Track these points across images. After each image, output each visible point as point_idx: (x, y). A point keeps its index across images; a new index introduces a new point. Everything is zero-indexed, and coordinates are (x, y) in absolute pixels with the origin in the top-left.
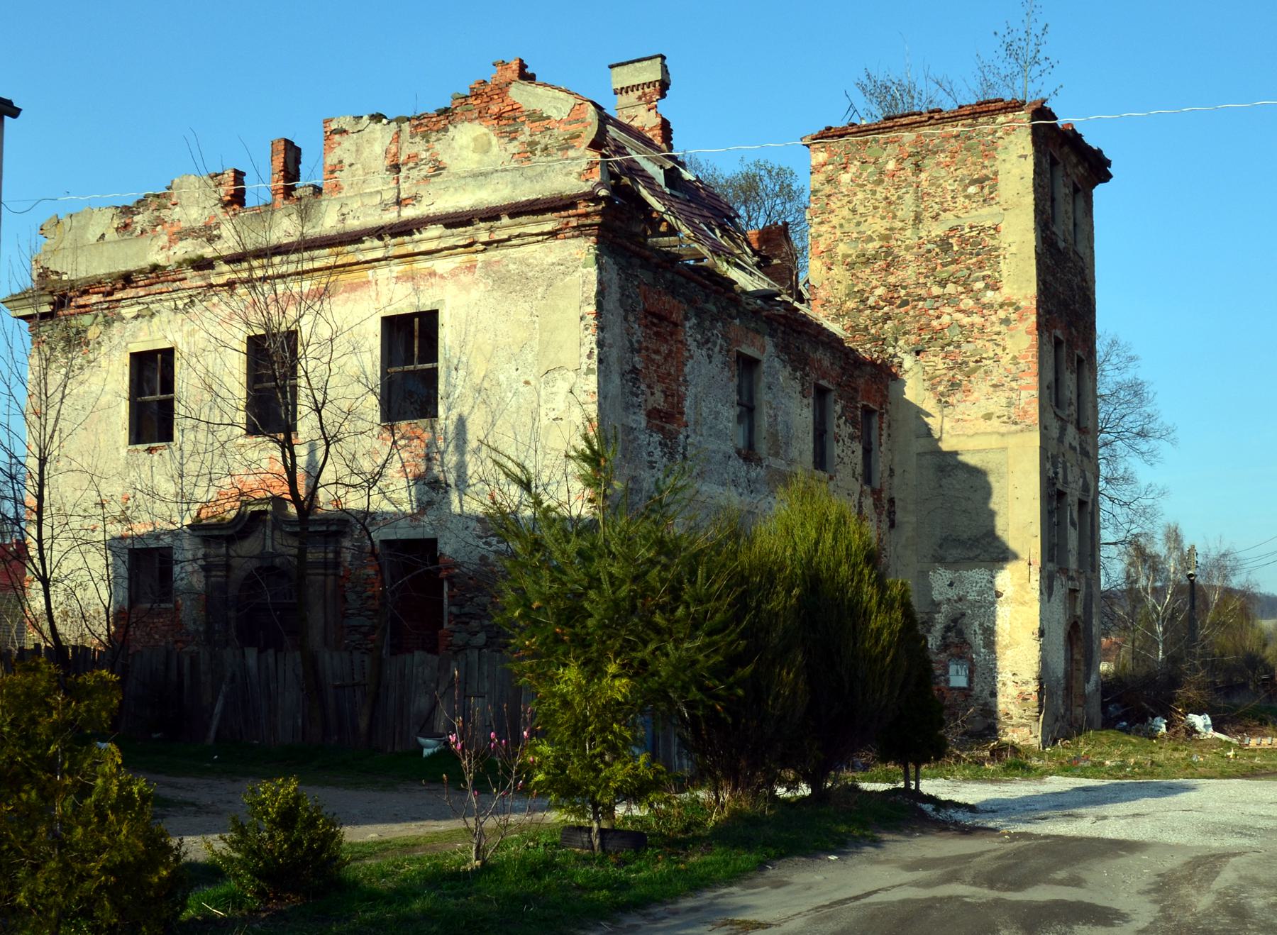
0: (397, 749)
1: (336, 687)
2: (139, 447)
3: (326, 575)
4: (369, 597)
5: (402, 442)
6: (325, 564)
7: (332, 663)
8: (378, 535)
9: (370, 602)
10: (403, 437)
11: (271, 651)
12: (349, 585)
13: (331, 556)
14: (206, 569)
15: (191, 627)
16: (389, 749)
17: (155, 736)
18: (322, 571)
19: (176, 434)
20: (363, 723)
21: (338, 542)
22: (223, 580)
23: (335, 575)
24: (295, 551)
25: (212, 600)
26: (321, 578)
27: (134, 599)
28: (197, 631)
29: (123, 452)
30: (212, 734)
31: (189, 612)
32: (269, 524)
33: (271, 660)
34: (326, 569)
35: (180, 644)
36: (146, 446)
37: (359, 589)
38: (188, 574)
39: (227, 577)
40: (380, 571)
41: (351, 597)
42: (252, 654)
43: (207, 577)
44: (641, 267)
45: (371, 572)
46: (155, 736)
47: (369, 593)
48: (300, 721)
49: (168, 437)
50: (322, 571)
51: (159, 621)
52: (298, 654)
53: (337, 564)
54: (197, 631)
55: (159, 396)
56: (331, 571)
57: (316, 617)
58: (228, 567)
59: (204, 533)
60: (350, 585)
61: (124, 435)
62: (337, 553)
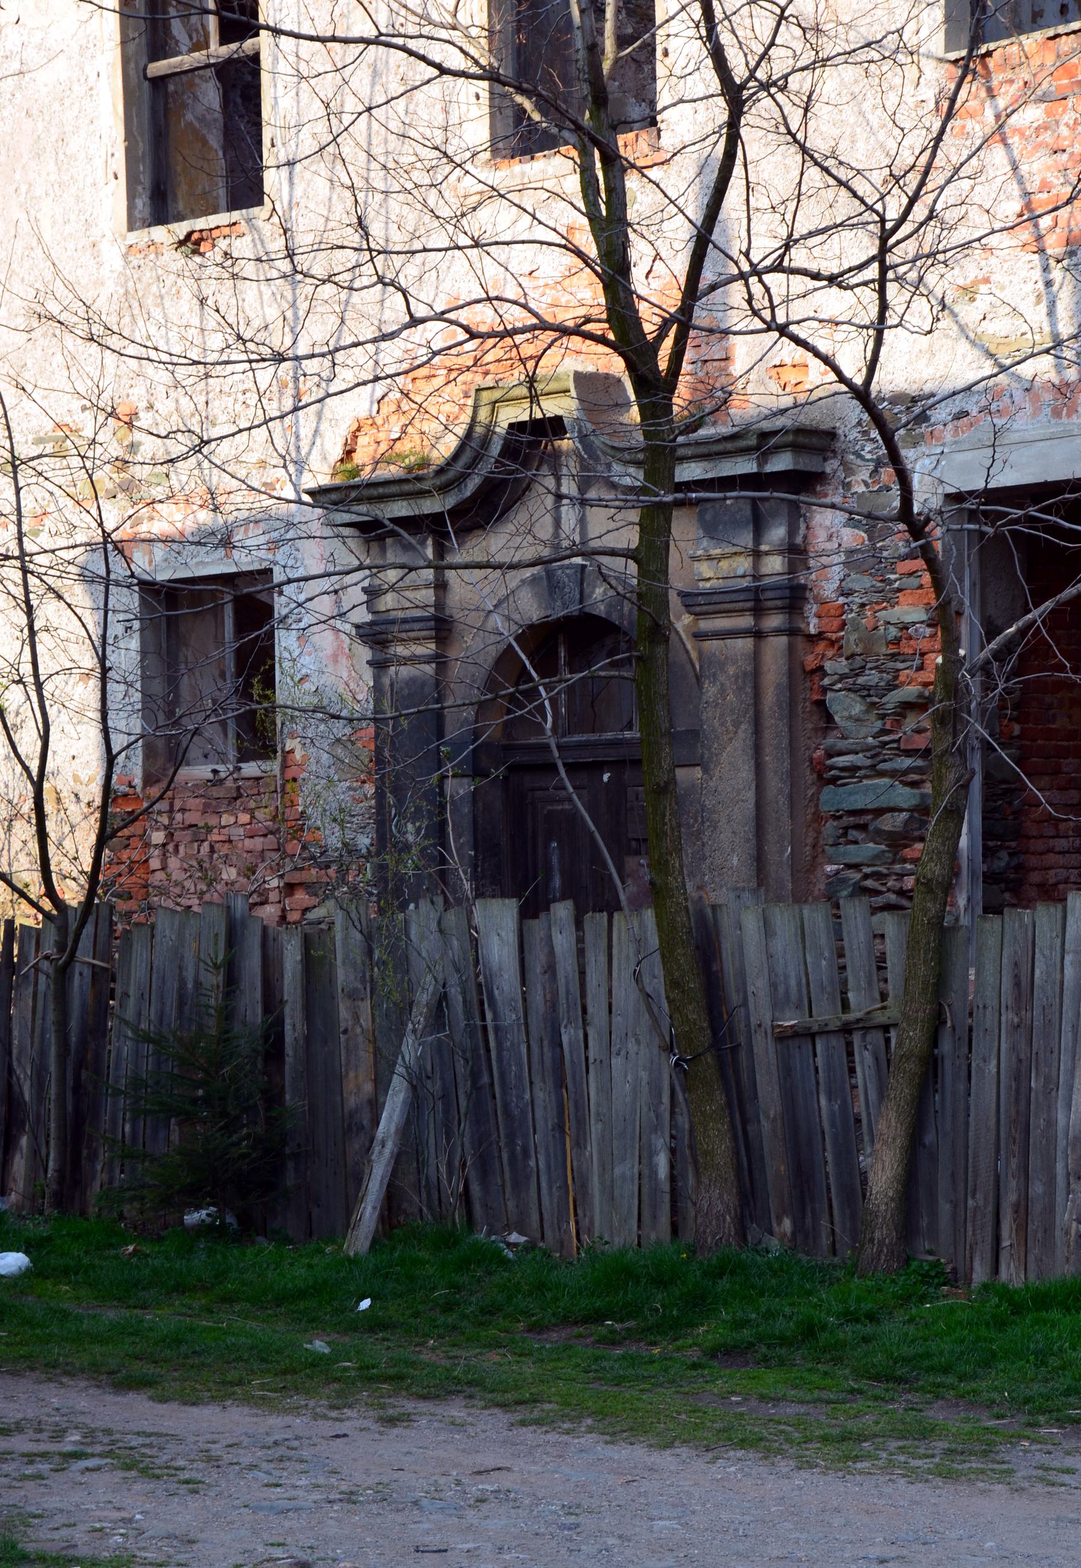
0: (1010, 1273)
1: (784, 1037)
2: (159, 233)
3: (758, 635)
4: (907, 707)
5: (1032, 115)
6: (755, 598)
7: (770, 948)
8: (940, 470)
9: (911, 722)
10: (1029, 94)
11: (562, 911)
12: (836, 666)
13: (774, 564)
14: (376, 635)
15: (333, 839)
16: (980, 1274)
17: (193, 1218)
18: (746, 621)
19: (272, 180)
20: (882, 1171)
21: (796, 515)
22: (429, 669)
23: (792, 632)
24: (631, 538)
25: (405, 736)
26: (744, 645)
27: (166, 752)
28: (349, 848)
29: (112, 256)
30: (369, 1211)
31: (326, 781)
32: (571, 466)
33: (563, 942)
34: (758, 611)
35: (301, 897)
36: (181, 229)
37: (871, 677)
38: (319, 660)
39: (440, 661)
40: (944, 618)
41: (846, 707)
42: (498, 921)
43: (379, 665)
44: (395, 1393)
45: (911, 610)
46: (193, 1218)
47: (910, 691)
48: (662, 1162)
49: (247, 191)
50: (746, 621)
51: (233, 822)
52: (649, 915)
53: (794, 597)
54: (349, 848)
55: (218, 51)
56: (774, 621)
57: (725, 783)
58: (441, 627)
59: (363, 512)
60: (841, 665)
61: (111, 198)
62: (797, 553)
